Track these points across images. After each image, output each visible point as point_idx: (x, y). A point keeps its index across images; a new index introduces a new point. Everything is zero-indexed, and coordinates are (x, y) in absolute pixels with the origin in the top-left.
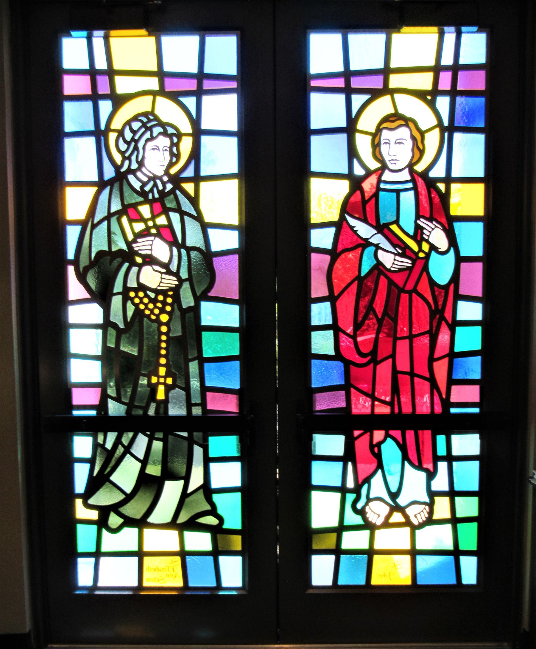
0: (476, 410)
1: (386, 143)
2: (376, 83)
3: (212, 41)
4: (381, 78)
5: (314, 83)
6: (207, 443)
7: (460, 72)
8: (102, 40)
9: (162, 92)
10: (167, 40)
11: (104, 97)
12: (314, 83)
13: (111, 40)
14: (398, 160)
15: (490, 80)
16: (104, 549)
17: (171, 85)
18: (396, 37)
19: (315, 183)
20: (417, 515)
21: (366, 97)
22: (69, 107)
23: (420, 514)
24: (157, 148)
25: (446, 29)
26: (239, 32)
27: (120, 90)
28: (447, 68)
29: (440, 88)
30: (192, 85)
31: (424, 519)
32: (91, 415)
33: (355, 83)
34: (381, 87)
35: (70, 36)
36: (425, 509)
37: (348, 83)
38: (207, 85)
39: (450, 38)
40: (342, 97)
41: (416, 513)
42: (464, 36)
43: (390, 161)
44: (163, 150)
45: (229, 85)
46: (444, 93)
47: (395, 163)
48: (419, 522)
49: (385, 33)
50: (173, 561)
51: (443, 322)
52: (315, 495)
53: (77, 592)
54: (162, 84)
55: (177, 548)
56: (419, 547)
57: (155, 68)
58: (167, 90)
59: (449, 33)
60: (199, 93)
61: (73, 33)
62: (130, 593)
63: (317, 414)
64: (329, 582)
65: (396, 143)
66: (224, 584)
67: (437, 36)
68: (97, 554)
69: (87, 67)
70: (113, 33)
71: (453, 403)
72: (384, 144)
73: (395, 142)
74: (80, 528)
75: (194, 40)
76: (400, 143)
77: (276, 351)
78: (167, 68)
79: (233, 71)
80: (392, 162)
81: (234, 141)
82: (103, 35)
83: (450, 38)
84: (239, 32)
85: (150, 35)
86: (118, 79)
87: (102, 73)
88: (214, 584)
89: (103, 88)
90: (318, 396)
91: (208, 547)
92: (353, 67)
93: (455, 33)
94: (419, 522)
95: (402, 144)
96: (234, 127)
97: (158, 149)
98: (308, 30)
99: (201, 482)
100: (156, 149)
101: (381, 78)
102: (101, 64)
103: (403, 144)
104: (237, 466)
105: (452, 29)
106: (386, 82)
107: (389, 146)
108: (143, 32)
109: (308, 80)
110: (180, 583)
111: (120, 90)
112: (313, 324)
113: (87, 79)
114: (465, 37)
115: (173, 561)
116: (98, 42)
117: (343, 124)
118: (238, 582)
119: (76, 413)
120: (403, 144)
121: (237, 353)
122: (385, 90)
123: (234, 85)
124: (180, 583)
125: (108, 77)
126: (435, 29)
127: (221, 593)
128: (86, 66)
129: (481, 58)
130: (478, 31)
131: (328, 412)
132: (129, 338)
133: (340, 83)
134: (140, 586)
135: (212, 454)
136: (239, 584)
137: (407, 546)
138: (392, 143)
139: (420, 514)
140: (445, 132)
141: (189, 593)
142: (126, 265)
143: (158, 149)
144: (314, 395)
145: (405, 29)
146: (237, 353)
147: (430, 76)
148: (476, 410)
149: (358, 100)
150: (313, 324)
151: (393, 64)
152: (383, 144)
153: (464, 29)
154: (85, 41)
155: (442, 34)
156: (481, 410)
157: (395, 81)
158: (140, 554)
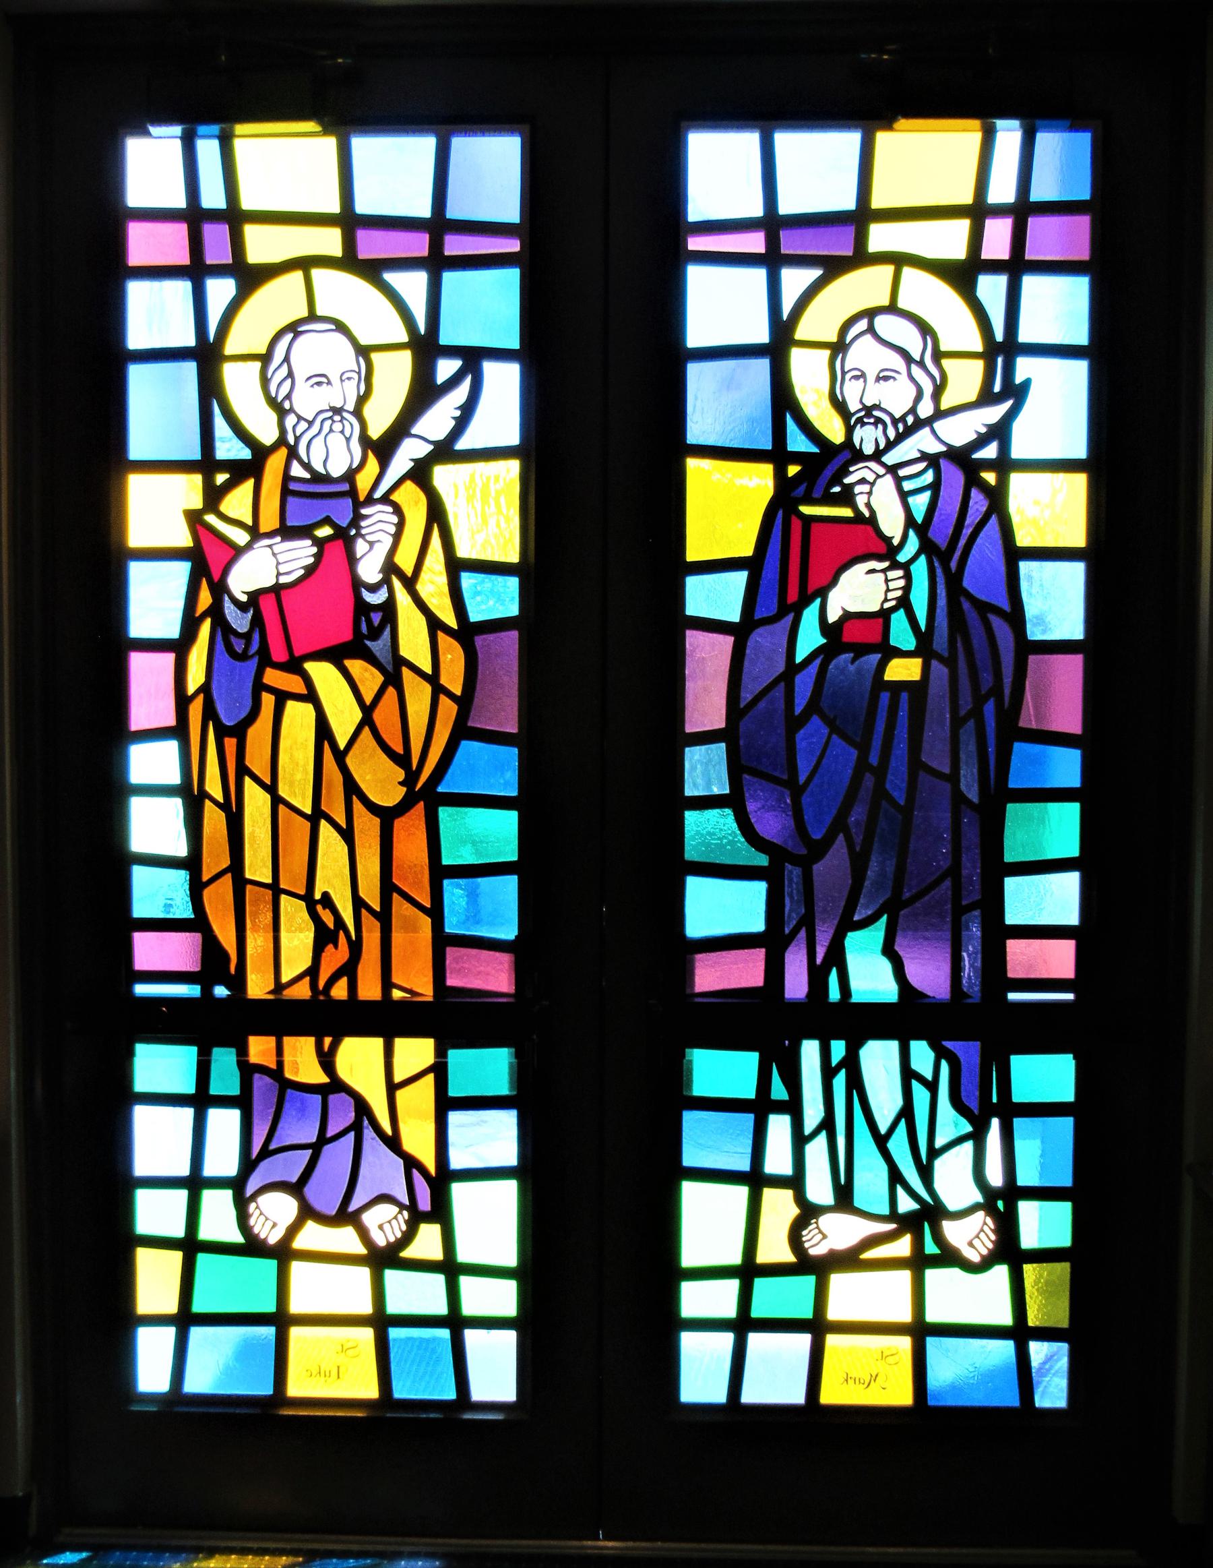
1: (856, 378)
2: (839, 244)
3: (465, 147)
4: (849, 232)
6: (444, 1060)
7: (1033, 219)
8: (215, 143)
9: (350, 261)
10: (364, 146)
11: (219, 271)
12: (696, 244)
13: (238, 144)
17: (371, 245)
18: (882, 138)
20: (973, 1242)
21: (815, 273)
22: (138, 293)
23: (979, 1238)
25: (1000, 123)
26: (527, 128)
27: (255, 255)
28: (999, 211)
29: (986, 255)
31: (399, 1235)
32: (163, 996)
33: (790, 243)
35: (147, 133)
36: (985, 1223)
38: (454, 246)
40: (759, 275)
41: (969, 1239)
46: (994, 267)
48: (267, 1237)
49: (860, 130)
51: (395, 895)
52: (690, 1191)
53: (136, 1408)
54: (349, 243)
55: (367, 1308)
56: (933, 1315)
57: (334, 207)
58: (361, 256)
61: (154, 130)
62: (257, 1411)
64: (717, 1394)
65: (878, 379)
67: (977, 137)
71: (209, 1053)
72: (853, 380)
73: (865, 381)
74: (143, 1255)
75: (423, 146)
76: (886, 378)
77: (989, 776)
78: (364, 205)
84: (527, 128)
85: (326, 131)
86: (251, 232)
87: (214, 216)
89: (217, 250)
92: (786, 207)
94: (267, 1237)
95: (892, 380)
98: (683, 124)
99: (891, 1145)
101: (849, 232)
102: (213, 197)
106: (861, 239)
108: (311, 126)
109: (682, 234)
110: (371, 1391)
111: (255, 255)
112: (689, 791)
113: (180, 231)
116: (208, 150)
117: (761, 334)
119: (141, 989)
122: (861, 258)
124: (371, 1391)
126: (976, 123)
127: (468, 1416)
131: (731, 997)
133: (755, 243)
134: (280, 1395)
137: (905, 1316)
138: (871, 377)
139: (979, 1238)
140: (997, 355)
145: (902, 123)
147: (962, 227)
148: (1070, 996)
149: (795, 280)
150: (689, 791)
152: (850, 380)
154: (178, 144)
155: (989, 136)
157: (880, 237)
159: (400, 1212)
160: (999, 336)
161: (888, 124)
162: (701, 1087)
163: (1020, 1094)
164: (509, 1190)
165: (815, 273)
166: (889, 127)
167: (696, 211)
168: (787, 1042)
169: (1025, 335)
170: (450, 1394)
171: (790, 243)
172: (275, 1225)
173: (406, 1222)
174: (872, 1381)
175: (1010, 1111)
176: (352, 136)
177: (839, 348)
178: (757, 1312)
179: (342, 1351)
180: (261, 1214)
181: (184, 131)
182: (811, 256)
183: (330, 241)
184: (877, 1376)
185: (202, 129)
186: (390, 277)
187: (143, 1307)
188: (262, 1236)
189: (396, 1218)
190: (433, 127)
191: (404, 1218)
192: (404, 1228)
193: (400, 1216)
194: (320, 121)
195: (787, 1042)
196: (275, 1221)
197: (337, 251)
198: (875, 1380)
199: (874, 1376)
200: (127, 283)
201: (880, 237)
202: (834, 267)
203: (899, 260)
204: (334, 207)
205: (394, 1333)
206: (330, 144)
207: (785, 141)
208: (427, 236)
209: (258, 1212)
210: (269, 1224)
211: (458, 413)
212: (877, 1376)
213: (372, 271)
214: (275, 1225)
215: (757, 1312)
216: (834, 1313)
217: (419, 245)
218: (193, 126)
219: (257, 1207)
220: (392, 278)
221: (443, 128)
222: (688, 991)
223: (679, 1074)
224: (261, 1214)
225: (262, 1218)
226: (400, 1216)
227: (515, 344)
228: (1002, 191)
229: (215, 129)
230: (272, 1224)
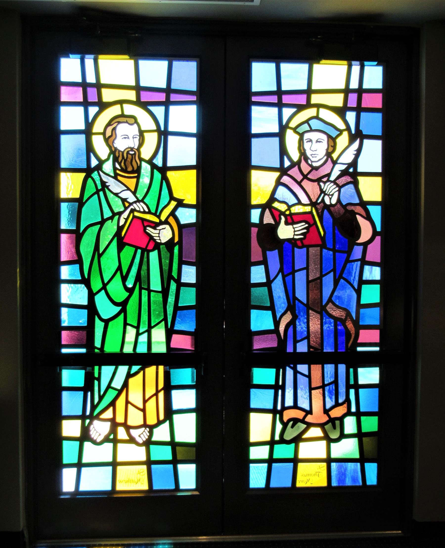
0: (377, 349)
2: (301, 100)
4: (304, 96)
5: (254, 99)
9: (139, 103)
11: (93, 104)
14: (318, 155)
15: (385, 101)
16: (84, 461)
17: (146, 97)
18: (316, 67)
19: (254, 174)
24: (127, 137)
25: (353, 63)
27: (105, 99)
28: (354, 91)
30: (162, 97)
32: (69, 353)
33: (286, 99)
34: (305, 104)
37: (280, 99)
38: (174, 97)
39: (356, 69)
40: (275, 110)
42: (366, 68)
43: (311, 155)
44: (133, 138)
45: (189, 99)
46: (352, 109)
47: (316, 157)
50: (140, 472)
52: (253, 416)
53: (62, 497)
54: (138, 96)
57: (133, 84)
59: (355, 65)
60: (167, 104)
61: (71, 56)
63: (254, 352)
66: (182, 487)
67: (346, 67)
68: (79, 465)
69: (80, 80)
70: (100, 57)
73: (317, 140)
74: (65, 444)
76: (320, 142)
78: (143, 83)
79: (194, 88)
80: (313, 156)
81: (194, 141)
82: (93, 58)
83: (356, 69)
84: (198, 59)
85: (131, 58)
86: (104, 91)
87: (91, 85)
88: (173, 487)
89: (92, 97)
90: (256, 338)
91: (169, 457)
93: (360, 66)
95: (321, 143)
96: (194, 130)
97: (128, 138)
100: (127, 138)
101: (304, 96)
102: (91, 79)
103: (322, 142)
104: (193, 392)
105: (358, 63)
106: (309, 99)
107: (311, 144)
108: (127, 57)
110: (145, 487)
111: (105, 99)
114: (367, 69)
115: (140, 472)
117: (82, 127)
118: (193, 486)
120: (322, 142)
121: (194, 303)
122: (308, 105)
123: (194, 98)
124: (145, 487)
125: (96, 89)
126: (345, 62)
127: (179, 494)
128: (79, 79)
129: (379, 85)
130: (377, 65)
131: (266, 351)
132: (317, 332)
133: (274, 99)
135: (274, 336)
136: (193, 486)
138: (314, 141)
141: (152, 495)
142: (146, 253)
143: (128, 138)
144: (252, 337)
145: (323, 61)
146: (194, 303)
148: (377, 349)
149: (287, 112)
151: (314, 87)
153: (366, 63)
156: (380, 349)
157: (315, 99)
158: (114, 464)
159: (146, 429)
160: (162, 129)
161: (318, 61)
162: (256, 381)
163: (361, 382)
164: (193, 416)
165: (294, 110)
166: (318, 62)
167: (255, 89)
168: (224, 376)
169: (170, 129)
170: (173, 487)
171: (286, 99)
172: (100, 435)
173: (148, 432)
174: (308, 481)
175: (357, 387)
176: (173, 61)
177: (141, 133)
178: (275, 456)
179: (139, 473)
180: (95, 430)
181: (94, 57)
182: (190, 101)
183: (132, 95)
184: (309, 480)
185: (87, 56)
186: (151, 108)
187: (65, 461)
188: (95, 439)
189: (144, 431)
190: (195, 59)
191: (147, 431)
192: (148, 434)
193: (146, 430)
194: (129, 55)
195: (224, 376)
196: (100, 433)
197: (134, 99)
198: (308, 481)
199: (308, 480)
200: (60, 106)
201: (315, 99)
202: (300, 108)
203: (318, 106)
204: (133, 84)
205: (153, 466)
206: (132, 62)
207: (284, 66)
208: (165, 94)
209: (94, 429)
210: (98, 434)
211: (355, 153)
212: (309, 480)
213: (144, 105)
214: (100, 435)
215: (275, 456)
216: (301, 456)
217: (162, 97)
218: (84, 55)
219: (94, 427)
220: (152, 108)
221: (171, 58)
222: (252, 349)
223: (249, 377)
224: (95, 430)
225: (95, 432)
226: (146, 430)
227: (380, 133)
228: (354, 85)
229: (92, 56)
230: (99, 434)
